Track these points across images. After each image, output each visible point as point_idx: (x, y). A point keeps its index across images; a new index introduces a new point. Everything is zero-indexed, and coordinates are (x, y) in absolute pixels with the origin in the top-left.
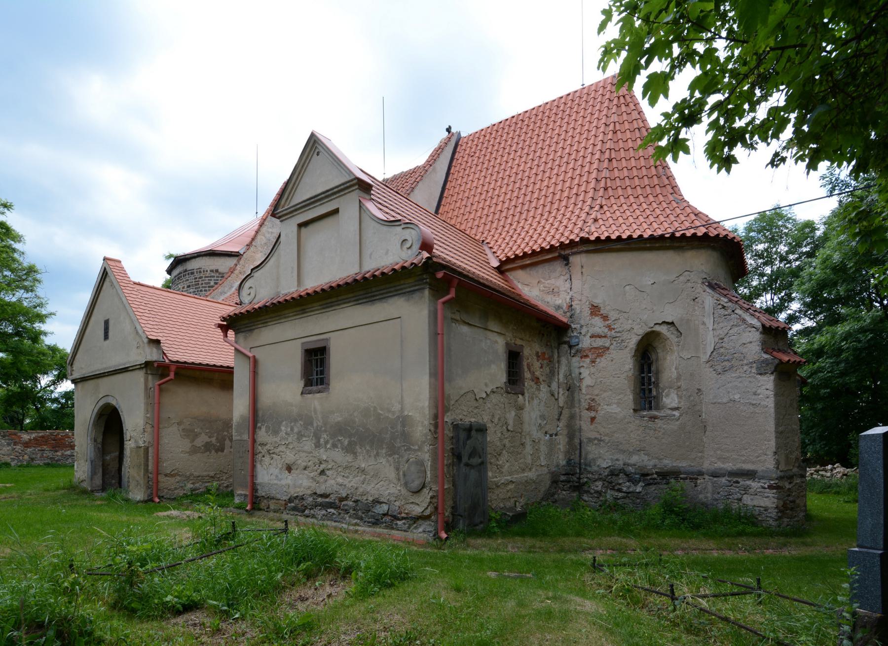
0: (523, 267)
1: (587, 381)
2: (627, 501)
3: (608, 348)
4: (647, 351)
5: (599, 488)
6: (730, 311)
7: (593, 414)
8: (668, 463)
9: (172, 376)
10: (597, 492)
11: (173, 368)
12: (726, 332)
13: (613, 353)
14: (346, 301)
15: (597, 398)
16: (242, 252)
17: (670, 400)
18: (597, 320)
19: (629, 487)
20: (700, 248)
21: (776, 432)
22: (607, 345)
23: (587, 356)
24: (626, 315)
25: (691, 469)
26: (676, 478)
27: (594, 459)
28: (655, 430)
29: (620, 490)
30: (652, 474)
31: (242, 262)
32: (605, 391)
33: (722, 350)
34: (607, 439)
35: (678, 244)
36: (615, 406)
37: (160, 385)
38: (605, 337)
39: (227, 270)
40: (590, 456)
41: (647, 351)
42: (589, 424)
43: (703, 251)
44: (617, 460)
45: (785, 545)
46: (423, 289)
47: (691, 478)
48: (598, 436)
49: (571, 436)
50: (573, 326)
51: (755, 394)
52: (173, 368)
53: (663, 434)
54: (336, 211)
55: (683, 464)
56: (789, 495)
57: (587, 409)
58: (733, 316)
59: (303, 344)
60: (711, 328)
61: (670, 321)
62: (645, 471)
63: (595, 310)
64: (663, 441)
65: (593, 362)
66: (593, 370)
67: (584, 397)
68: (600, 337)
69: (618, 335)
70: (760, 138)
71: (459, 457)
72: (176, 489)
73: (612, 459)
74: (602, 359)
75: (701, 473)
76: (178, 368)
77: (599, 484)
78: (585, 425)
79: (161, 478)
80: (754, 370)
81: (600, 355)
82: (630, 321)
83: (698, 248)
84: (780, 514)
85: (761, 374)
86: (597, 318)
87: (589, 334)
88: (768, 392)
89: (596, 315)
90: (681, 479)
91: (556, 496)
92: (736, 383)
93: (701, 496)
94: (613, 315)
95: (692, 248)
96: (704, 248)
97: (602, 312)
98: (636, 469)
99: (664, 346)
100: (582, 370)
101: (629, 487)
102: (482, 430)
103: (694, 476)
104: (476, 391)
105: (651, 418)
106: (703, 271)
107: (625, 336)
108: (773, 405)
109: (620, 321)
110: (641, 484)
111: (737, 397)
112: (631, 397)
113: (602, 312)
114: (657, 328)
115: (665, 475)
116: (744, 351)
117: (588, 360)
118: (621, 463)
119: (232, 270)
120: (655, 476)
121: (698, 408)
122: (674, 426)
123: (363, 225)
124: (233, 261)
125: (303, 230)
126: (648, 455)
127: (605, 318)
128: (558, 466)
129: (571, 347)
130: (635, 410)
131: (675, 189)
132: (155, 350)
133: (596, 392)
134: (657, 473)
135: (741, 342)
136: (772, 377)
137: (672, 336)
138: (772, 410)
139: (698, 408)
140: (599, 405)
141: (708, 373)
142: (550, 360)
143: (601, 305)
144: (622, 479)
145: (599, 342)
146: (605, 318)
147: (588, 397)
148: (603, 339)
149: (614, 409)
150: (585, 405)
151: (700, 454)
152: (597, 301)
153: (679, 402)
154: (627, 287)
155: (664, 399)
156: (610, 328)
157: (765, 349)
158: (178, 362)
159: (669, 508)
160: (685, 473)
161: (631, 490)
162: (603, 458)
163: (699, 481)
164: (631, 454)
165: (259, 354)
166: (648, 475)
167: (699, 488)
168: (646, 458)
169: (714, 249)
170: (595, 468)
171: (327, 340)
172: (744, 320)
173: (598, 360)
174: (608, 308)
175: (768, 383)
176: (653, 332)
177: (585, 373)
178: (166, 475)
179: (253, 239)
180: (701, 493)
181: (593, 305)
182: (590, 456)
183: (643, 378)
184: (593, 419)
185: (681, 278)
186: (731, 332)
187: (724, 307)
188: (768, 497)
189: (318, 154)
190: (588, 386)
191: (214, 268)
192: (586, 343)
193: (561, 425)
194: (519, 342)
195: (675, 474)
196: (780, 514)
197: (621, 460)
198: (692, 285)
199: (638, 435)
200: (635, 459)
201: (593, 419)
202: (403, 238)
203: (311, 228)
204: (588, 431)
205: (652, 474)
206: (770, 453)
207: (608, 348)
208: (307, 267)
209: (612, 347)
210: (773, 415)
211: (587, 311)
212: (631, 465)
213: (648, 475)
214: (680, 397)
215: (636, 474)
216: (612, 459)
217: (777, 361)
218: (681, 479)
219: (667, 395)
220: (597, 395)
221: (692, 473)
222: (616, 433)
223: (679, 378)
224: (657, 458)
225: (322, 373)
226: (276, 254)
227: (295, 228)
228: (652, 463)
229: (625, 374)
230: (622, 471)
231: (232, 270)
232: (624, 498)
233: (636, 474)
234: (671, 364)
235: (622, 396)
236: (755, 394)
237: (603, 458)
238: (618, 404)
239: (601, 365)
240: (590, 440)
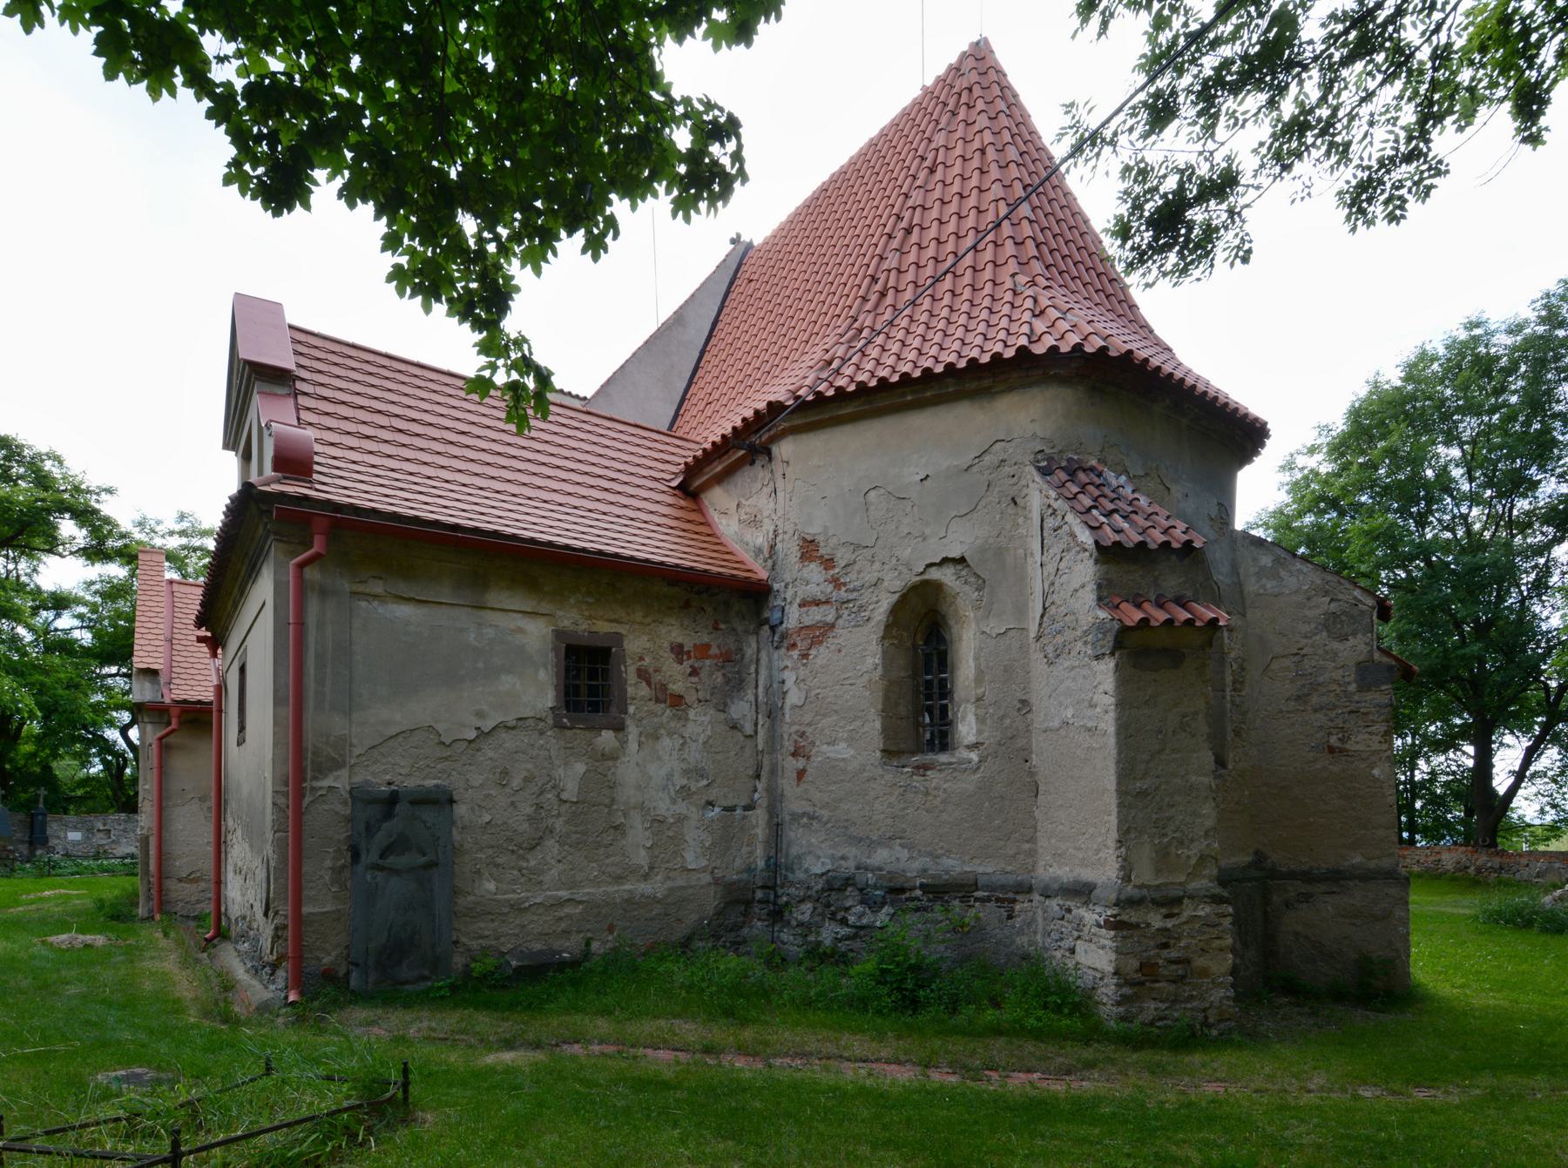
0: (720, 479)
2: (857, 944)
3: (832, 626)
4: (922, 627)
5: (806, 917)
7: (801, 763)
8: (954, 866)
10: (801, 924)
11: (174, 712)
13: (843, 636)
15: (809, 730)
17: (967, 728)
18: (814, 571)
19: (861, 916)
20: (1030, 385)
21: (1121, 792)
22: (830, 619)
24: (868, 553)
25: (1003, 880)
26: (965, 899)
27: (799, 857)
28: (927, 794)
29: (844, 922)
30: (912, 889)
32: (825, 716)
34: (825, 813)
35: (973, 385)
36: (843, 745)
37: (160, 739)
38: (827, 602)
40: (794, 851)
41: (922, 627)
42: (794, 783)
43: (1035, 390)
44: (843, 858)
45: (1090, 1065)
47: (998, 900)
48: (810, 809)
49: (772, 811)
50: (776, 586)
52: (174, 712)
53: (944, 802)
55: (986, 868)
56: (1165, 946)
57: (794, 755)
61: (955, 554)
62: (898, 883)
63: (809, 550)
64: (944, 816)
65: (805, 656)
66: (803, 672)
67: (788, 730)
68: (817, 603)
69: (855, 594)
70: (99, 35)
71: (356, 856)
72: (198, 902)
73: (833, 857)
74: (822, 649)
75: (1025, 889)
76: (184, 711)
77: (807, 907)
78: (787, 784)
79: (171, 884)
81: (816, 641)
82: (877, 565)
83: (1023, 386)
84: (1127, 990)
86: (813, 566)
87: (798, 600)
90: (976, 900)
91: (746, 931)
93: (1022, 941)
95: (1011, 389)
96: (1036, 383)
97: (822, 551)
98: (880, 877)
101: (861, 916)
102: (442, 800)
103: (1010, 894)
104: (440, 727)
105: (918, 767)
106: (1034, 435)
107: (867, 596)
108: (1112, 729)
109: (856, 567)
110: (887, 909)
112: (878, 725)
113: (822, 551)
114: (934, 574)
115: (938, 891)
117: (795, 653)
118: (851, 864)
120: (918, 893)
121: (1020, 742)
122: (969, 783)
126: (910, 847)
127: (828, 563)
128: (749, 870)
129: (773, 629)
130: (887, 753)
132: (147, 685)
133: (808, 718)
134: (922, 886)
136: (1112, 664)
137: (967, 588)
138: (1112, 741)
139: (1020, 742)
140: (813, 743)
142: (729, 658)
143: (820, 539)
144: (850, 898)
145: (816, 615)
146: (828, 563)
147: (795, 728)
148: (823, 608)
149: (842, 751)
150: (789, 746)
151: (1027, 846)
152: (813, 530)
153: (979, 732)
154: (872, 494)
156: (836, 583)
157: (1106, 594)
158: (185, 701)
159: (937, 965)
160: (987, 888)
161: (864, 921)
162: (816, 855)
163: (1018, 907)
164: (872, 845)
166: (902, 890)
167: (1018, 922)
168: (905, 854)
169: (1064, 381)
170: (800, 875)
173: (813, 652)
174: (833, 541)
175: (1105, 673)
176: (926, 584)
177: (790, 677)
178: (180, 880)
180: (1021, 932)
181: (804, 540)
182: (794, 851)
183: (929, 684)
184: (801, 774)
185: (987, 458)
186: (1062, 565)
188: (1103, 947)
190: (794, 707)
192: (794, 617)
193: (760, 786)
194: (603, 627)
195: (964, 889)
196: (1127, 990)
197: (851, 858)
198: (1012, 470)
199: (891, 805)
200: (881, 856)
201: (801, 774)
204: (795, 800)
205: (912, 889)
206: (1112, 843)
207: (832, 626)
209: (840, 622)
210: (1114, 752)
211: (795, 554)
212: (873, 870)
213: (902, 890)
215: (875, 887)
216: (833, 857)
217: (1117, 626)
218: (976, 900)
220: (809, 724)
221: (1003, 888)
222: (852, 805)
224: (930, 854)
228: (917, 865)
229: (866, 677)
230: (848, 881)
232: (847, 938)
233: (875, 887)
235: (858, 723)
237: (816, 855)
238: (851, 741)
239: (819, 661)
240: (796, 817)
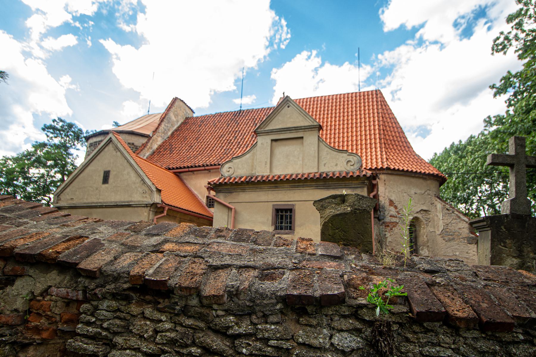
1: (389, 239)
4: (414, 225)
6: (451, 212)
9: (165, 213)
11: (167, 208)
12: (449, 221)
14: (310, 186)
16: (151, 135)
18: (392, 208)
22: (398, 221)
23: (388, 226)
31: (151, 141)
33: (447, 230)
39: (140, 145)
41: (414, 225)
46: (364, 187)
51: (467, 253)
54: (302, 138)
58: (453, 214)
59: (273, 205)
60: (441, 219)
63: (391, 203)
65: (392, 229)
68: (394, 217)
80: (466, 241)
81: (394, 226)
85: (470, 244)
88: (474, 253)
89: (392, 206)
92: (456, 247)
94: (399, 207)
99: (420, 225)
100: (386, 233)
111: (457, 253)
116: (460, 232)
117: (389, 228)
119: (144, 145)
123: (320, 149)
124: (144, 140)
125: (274, 143)
127: (396, 207)
131: (410, 147)
135: (458, 227)
141: (440, 239)
145: (394, 220)
146: (396, 207)
155: (420, 251)
165: (238, 207)
171: (293, 205)
172: (459, 217)
177: (388, 235)
179: (157, 129)
187: (447, 209)
189: (288, 107)
191: (131, 142)
192: (388, 219)
202: (348, 160)
203: (279, 143)
208: (275, 163)
211: (387, 203)
214: (429, 251)
219: (422, 250)
223: (428, 241)
225: (291, 223)
226: (252, 152)
227: (270, 142)
231: (144, 145)
234: (424, 233)
236: (467, 253)
